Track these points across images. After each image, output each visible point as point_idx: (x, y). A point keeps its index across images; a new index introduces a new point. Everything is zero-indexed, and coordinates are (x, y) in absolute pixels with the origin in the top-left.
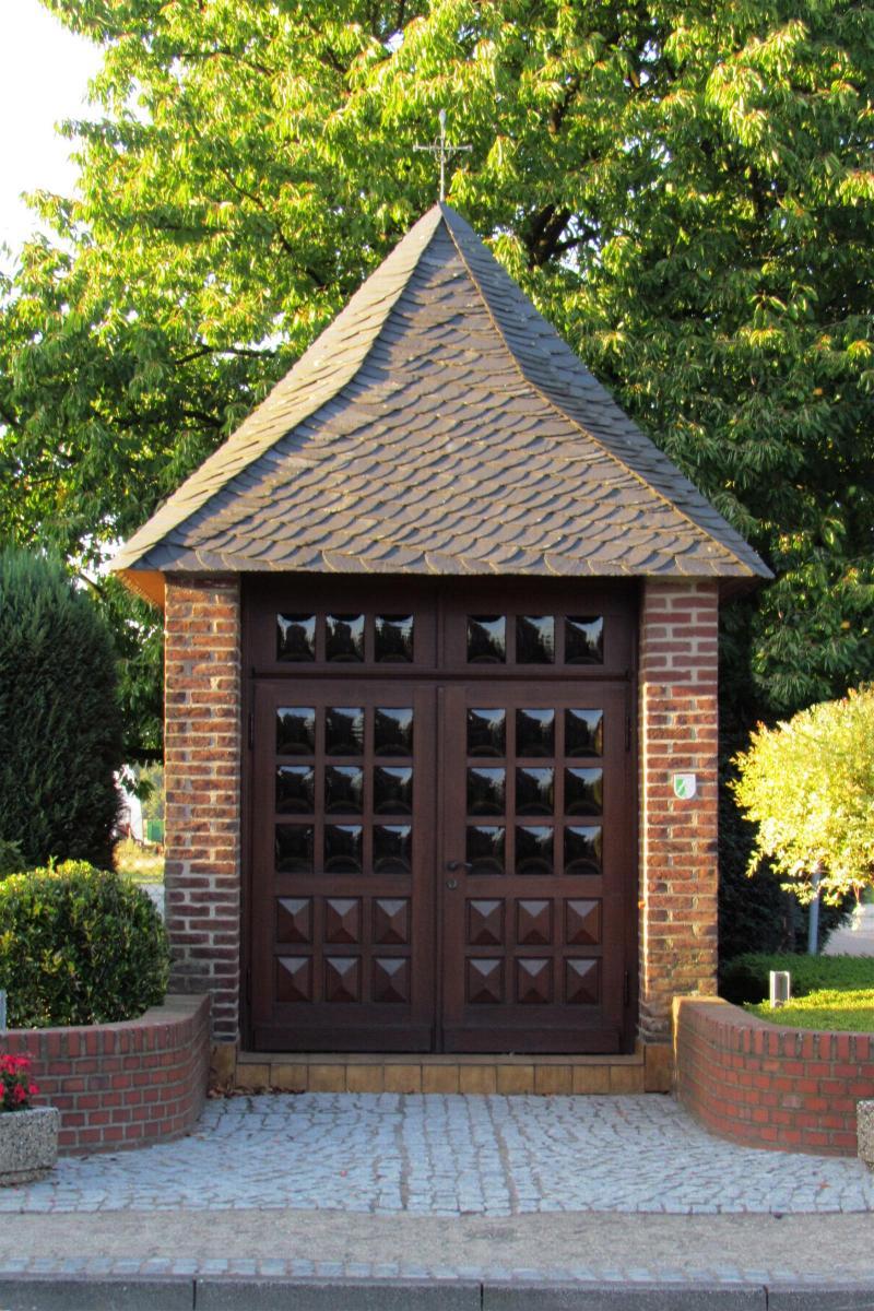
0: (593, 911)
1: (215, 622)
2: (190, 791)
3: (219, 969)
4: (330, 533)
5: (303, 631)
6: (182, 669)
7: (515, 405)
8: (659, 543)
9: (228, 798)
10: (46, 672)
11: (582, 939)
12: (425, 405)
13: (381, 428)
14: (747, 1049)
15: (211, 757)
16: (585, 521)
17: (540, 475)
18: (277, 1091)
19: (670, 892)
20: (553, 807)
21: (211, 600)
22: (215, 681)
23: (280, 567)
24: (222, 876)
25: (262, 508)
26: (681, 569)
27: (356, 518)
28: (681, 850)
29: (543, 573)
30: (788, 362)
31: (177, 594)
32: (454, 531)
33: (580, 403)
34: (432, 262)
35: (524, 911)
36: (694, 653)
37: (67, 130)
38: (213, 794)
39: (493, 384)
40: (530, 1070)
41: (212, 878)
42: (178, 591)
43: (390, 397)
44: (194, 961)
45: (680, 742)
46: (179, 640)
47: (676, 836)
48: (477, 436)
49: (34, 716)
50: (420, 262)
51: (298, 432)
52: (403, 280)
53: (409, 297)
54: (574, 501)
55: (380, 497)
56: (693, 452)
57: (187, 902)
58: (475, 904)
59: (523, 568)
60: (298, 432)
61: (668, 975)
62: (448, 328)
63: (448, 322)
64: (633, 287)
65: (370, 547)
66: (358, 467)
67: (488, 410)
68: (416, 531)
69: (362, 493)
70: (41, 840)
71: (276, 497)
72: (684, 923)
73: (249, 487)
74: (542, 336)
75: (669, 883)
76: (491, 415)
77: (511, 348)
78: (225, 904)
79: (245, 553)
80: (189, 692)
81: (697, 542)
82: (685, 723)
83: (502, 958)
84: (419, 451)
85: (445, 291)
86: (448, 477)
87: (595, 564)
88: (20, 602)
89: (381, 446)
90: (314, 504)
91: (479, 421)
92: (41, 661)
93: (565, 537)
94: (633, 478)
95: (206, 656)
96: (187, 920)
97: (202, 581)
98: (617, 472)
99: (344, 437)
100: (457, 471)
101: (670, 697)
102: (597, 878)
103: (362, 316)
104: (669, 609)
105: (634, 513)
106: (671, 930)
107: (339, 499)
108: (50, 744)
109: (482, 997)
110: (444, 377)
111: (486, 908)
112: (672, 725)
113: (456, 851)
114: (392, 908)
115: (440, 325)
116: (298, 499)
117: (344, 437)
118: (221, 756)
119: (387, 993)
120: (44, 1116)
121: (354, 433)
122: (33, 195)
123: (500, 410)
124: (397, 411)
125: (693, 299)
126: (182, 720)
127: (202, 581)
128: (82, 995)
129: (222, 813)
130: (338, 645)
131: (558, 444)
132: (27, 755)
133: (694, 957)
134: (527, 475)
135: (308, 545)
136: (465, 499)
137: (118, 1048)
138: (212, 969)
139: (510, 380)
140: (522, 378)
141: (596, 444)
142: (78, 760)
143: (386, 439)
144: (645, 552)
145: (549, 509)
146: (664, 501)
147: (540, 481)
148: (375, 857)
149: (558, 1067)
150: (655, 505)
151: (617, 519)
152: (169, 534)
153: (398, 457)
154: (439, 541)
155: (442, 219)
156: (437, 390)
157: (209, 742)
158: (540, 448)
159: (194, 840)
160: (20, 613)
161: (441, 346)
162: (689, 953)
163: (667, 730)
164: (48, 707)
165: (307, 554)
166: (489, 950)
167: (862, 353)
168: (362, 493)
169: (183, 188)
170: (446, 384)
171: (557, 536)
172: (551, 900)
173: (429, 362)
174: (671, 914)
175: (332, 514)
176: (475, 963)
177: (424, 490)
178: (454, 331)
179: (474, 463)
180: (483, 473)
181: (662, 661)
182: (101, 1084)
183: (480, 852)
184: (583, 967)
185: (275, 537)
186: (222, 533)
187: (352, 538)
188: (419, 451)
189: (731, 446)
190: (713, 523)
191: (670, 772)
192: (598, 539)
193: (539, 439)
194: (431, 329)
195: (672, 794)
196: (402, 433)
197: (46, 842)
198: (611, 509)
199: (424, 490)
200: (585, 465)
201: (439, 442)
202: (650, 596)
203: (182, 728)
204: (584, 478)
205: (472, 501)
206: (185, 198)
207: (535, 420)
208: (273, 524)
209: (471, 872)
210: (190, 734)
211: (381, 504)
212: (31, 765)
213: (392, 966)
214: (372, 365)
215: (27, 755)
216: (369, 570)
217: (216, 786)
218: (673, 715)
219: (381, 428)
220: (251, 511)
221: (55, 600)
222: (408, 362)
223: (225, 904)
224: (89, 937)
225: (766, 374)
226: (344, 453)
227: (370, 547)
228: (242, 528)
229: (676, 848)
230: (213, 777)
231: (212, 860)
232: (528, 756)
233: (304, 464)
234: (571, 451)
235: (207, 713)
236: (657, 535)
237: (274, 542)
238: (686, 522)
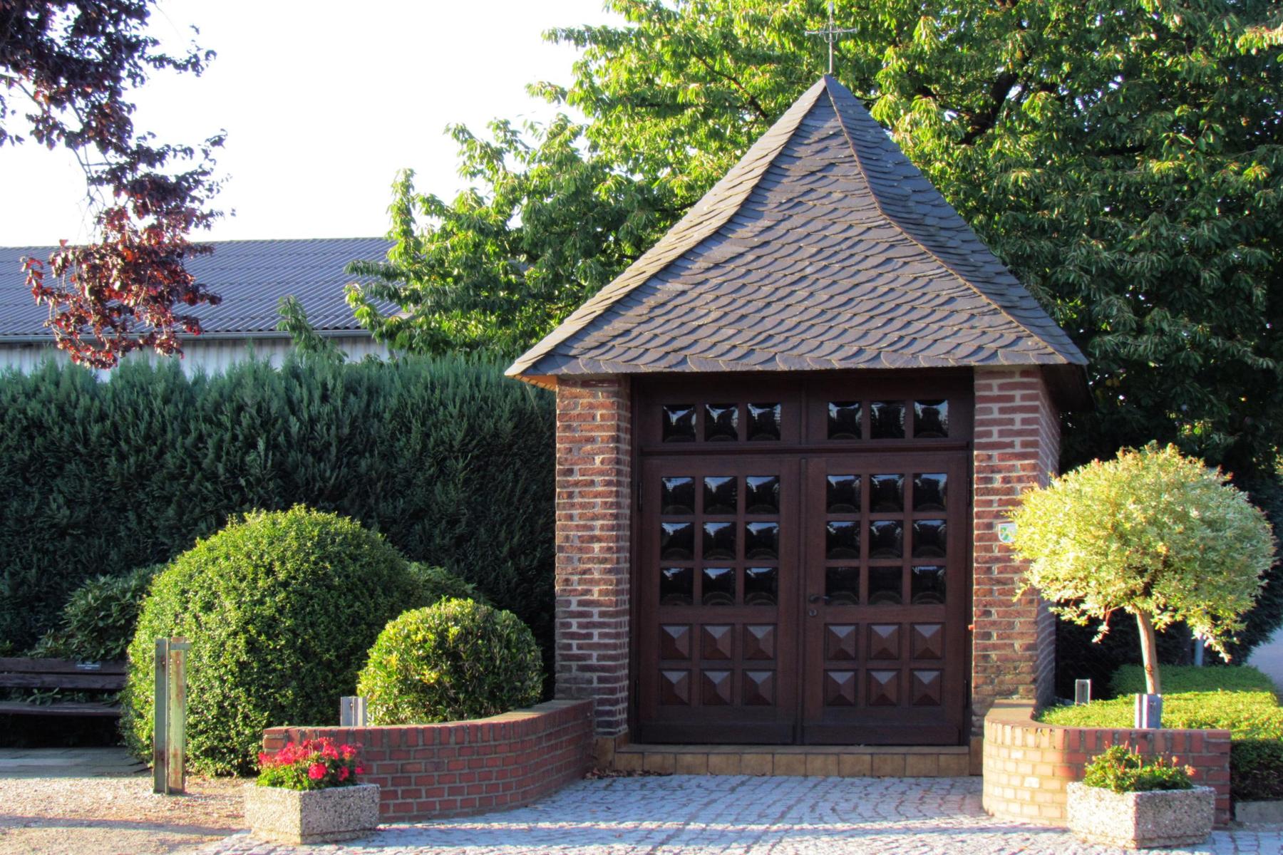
0: (937, 632)
1: (598, 413)
2: (577, 543)
3: (601, 680)
4: (696, 341)
5: (937, 413)
6: (570, 450)
7: (871, 234)
8: (985, 339)
9: (609, 549)
10: (516, 454)
11: (884, 655)
12: (791, 237)
13: (750, 257)
14: (999, 741)
15: (595, 518)
16: (922, 324)
17: (886, 289)
18: (646, 773)
19: (995, 617)
20: (858, 551)
21: (595, 396)
22: (598, 459)
23: (649, 369)
24: (604, 609)
25: (639, 324)
26: (1002, 360)
27: (720, 328)
28: (1005, 584)
29: (878, 367)
30: (1196, 187)
31: (566, 393)
32: (803, 336)
33: (932, 229)
34: (811, 123)
35: (876, 634)
36: (1018, 426)
37: (553, 36)
38: (597, 546)
39: (851, 218)
40: (868, 758)
41: (596, 610)
42: (568, 390)
43: (762, 232)
44: (580, 674)
45: (1004, 498)
46: (568, 428)
47: (1000, 572)
48: (833, 260)
49: (503, 489)
50: (801, 124)
51: (678, 263)
52: (784, 139)
53: (788, 153)
54: (913, 308)
55: (743, 311)
56: (1089, 264)
57: (574, 629)
58: (833, 628)
59: (861, 363)
60: (678, 263)
61: (992, 682)
62: (820, 175)
63: (820, 171)
64: (1057, 131)
65: (728, 351)
66: (726, 288)
67: (846, 239)
68: (771, 336)
69: (727, 309)
70: (509, 583)
71: (652, 315)
72: (1007, 641)
73: (631, 308)
74: (906, 177)
75: (993, 610)
76: (849, 243)
77: (872, 189)
78: (607, 630)
79: (710, 354)
80: (576, 468)
81: (1019, 338)
82: (1009, 482)
83: (855, 671)
84: (781, 274)
85: (821, 146)
86: (804, 293)
87: (924, 358)
88: (493, 401)
89: (749, 271)
90: (684, 319)
91: (837, 248)
92: (510, 447)
93: (901, 338)
94: (969, 289)
95: (591, 440)
96: (574, 643)
97: (588, 382)
98: (954, 284)
99: (717, 266)
100: (812, 288)
101: (996, 462)
102: (942, 606)
103: (747, 169)
104: (996, 392)
105: (965, 316)
106: (995, 647)
107: (706, 315)
108: (518, 510)
109: (836, 700)
110: (810, 214)
111: (842, 631)
112: (997, 484)
113: (817, 587)
114: (760, 632)
115: (813, 173)
116: (671, 316)
117: (717, 266)
118: (604, 517)
119: (754, 697)
120: (367, 791)
121: (726, 262)
122: (537, 87)
123: (857, 239)
124: (766, 243)
125: (1113, 140)
126: (571, 489)
127: (588, 382)
128: (456, 700)
129: (604, 561)
130: (721, 430)
131: (905, 263)
132: (498, 518)
133: (1015, 668)
134: (875, 289)
135: (675, 351)
136: (817, 310)
137: (453, 740)
138: (595, 680)
139: (867, 212)
140: (879, 212)
141: (939, 263)
142: (541, 522)
143: (754, 265)
144: (972, 346)
145: (889, 316)
146: (994, 306)
147: (886, 293)
148: (746, 593)
149: (892, 756)
150: (985, 309)
151: (950, 321)
152: (557, 346)
153: (762, 279)
154: (790, 344)
155: (825, 89)
156: (803, 225)
157: (593, 506)
158: (889, 267)
159: (580, 582)
160: (493, 409)
161: (812, 190)
162: (1010, 665)
163: (992, 489)
164: (516, 482)
165: (672, 359)
166: (844, 664)
167: (1257, 177)
168: (727, 309)
169: (664, 73)
170: (812, 220)
171: (895, 336)
172: (857, 625)
173: (800, 203)
174: (995, 635)
175: (700, 326)
176: (832, 675)
177: (781, 305)
178: (824, 177)
179: (828, 281)
180: (835, 289)
181: (989, 434)
182: (437, 767)
183: (840, 586)
184: (927, 677)
185: (648, 346)
186: (602, 344)
187: (715, 344)
188: (781, 274)
189: (1127, 257)
190: (1038, 322)
191: (995, 521)
192: (930, 339)
193: (889, 260)
194: (804, 177)
195: (996, 539)
196: (768, 260)
197: (513, 585)
198: (946, 313)
199: (781, 305)
200: (927, 279)
201: (800, 266)
202: (978, 382)
203: (570, 495)
204: (924, 290)
205: (823, 312)
206: (665, 81)
207: (887, 245)
208: (647, 335)
209: (827, 603)
210: (577, 500)
211: (743, 317)
212: (501, 525)
213: (760, 677)
214: (749, 208)
215: (498, 518)
216: (725, 368)
217: (599, 540)
218: (998, 477)
219: (750, 257)
220: (629, 326)
221: (524, 399)
222: (781, 204)
223: (607, 630)
224: (464, 656)
225: (1169, 200)
226: (715, 278)
227: (728, 351)
228: (620, 340)
229: (999, 582)
230: (597, 533)
231: (596, 596)
232: (881, 511)
233: (680, 287)
234: (917, 267)
235: (592, 483)
236: (984, 333)
237: (647, 350)
238: (1011, 322)
